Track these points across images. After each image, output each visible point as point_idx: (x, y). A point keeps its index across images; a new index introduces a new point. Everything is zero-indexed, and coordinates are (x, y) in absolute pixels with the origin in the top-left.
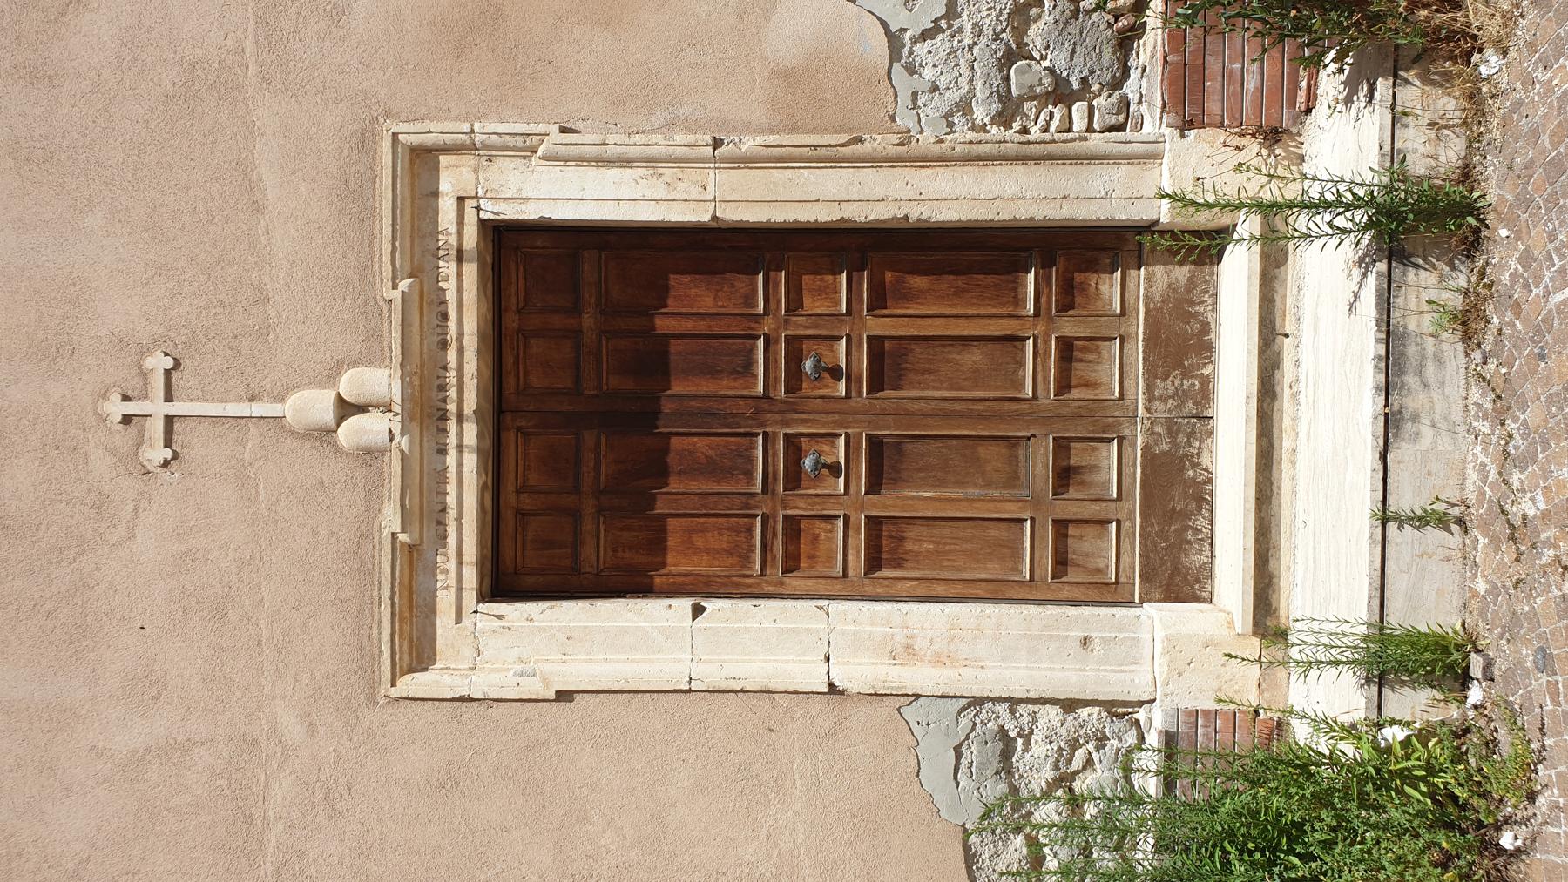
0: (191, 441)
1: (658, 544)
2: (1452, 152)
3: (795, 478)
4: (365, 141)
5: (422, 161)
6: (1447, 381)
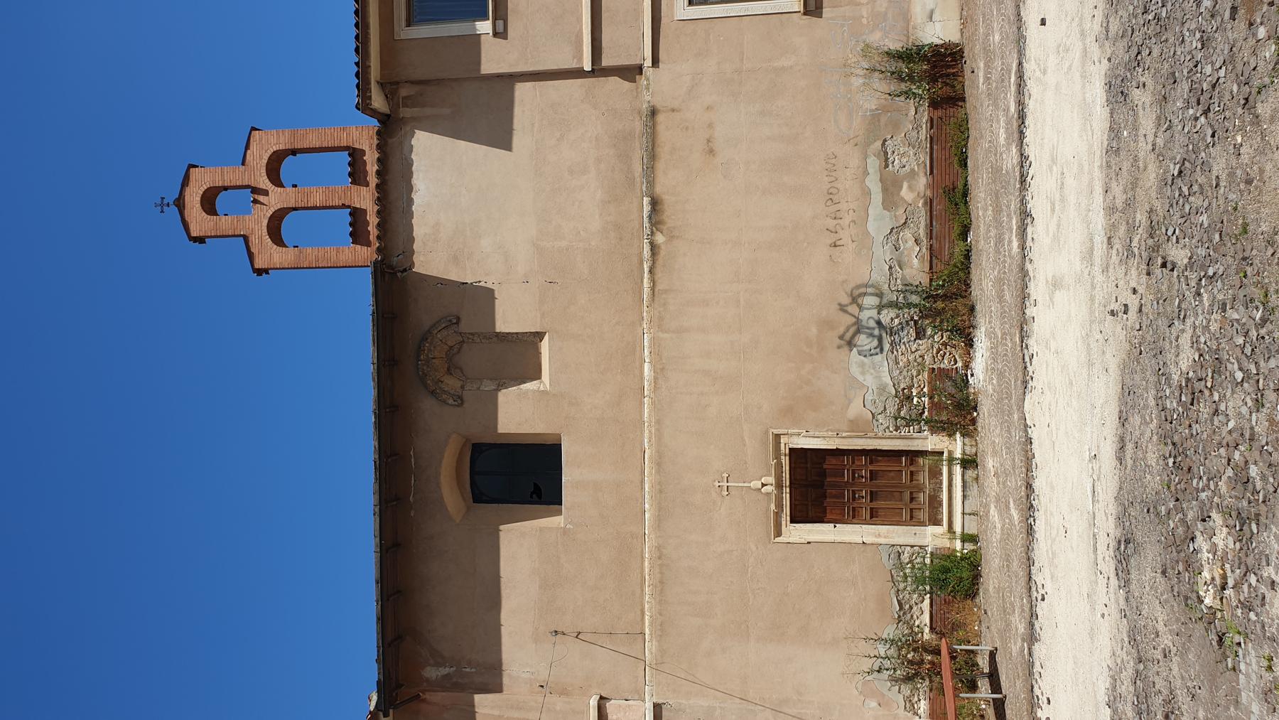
0: (733, 492)
1: (825, 512)
2: (974, 450)
3: (854, 499)
4: (767, 432)
5: (777, 437)
6: (974, 491)
